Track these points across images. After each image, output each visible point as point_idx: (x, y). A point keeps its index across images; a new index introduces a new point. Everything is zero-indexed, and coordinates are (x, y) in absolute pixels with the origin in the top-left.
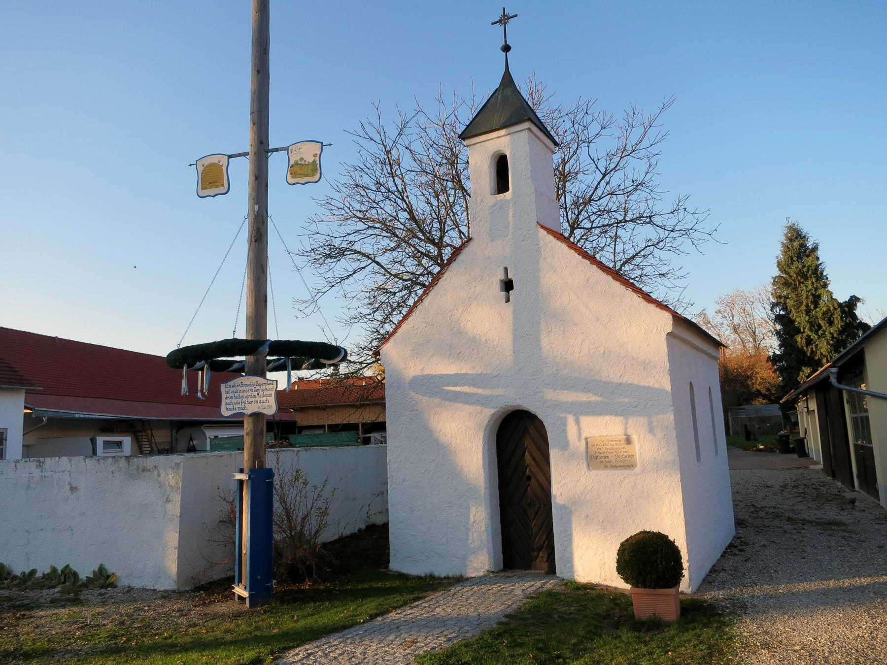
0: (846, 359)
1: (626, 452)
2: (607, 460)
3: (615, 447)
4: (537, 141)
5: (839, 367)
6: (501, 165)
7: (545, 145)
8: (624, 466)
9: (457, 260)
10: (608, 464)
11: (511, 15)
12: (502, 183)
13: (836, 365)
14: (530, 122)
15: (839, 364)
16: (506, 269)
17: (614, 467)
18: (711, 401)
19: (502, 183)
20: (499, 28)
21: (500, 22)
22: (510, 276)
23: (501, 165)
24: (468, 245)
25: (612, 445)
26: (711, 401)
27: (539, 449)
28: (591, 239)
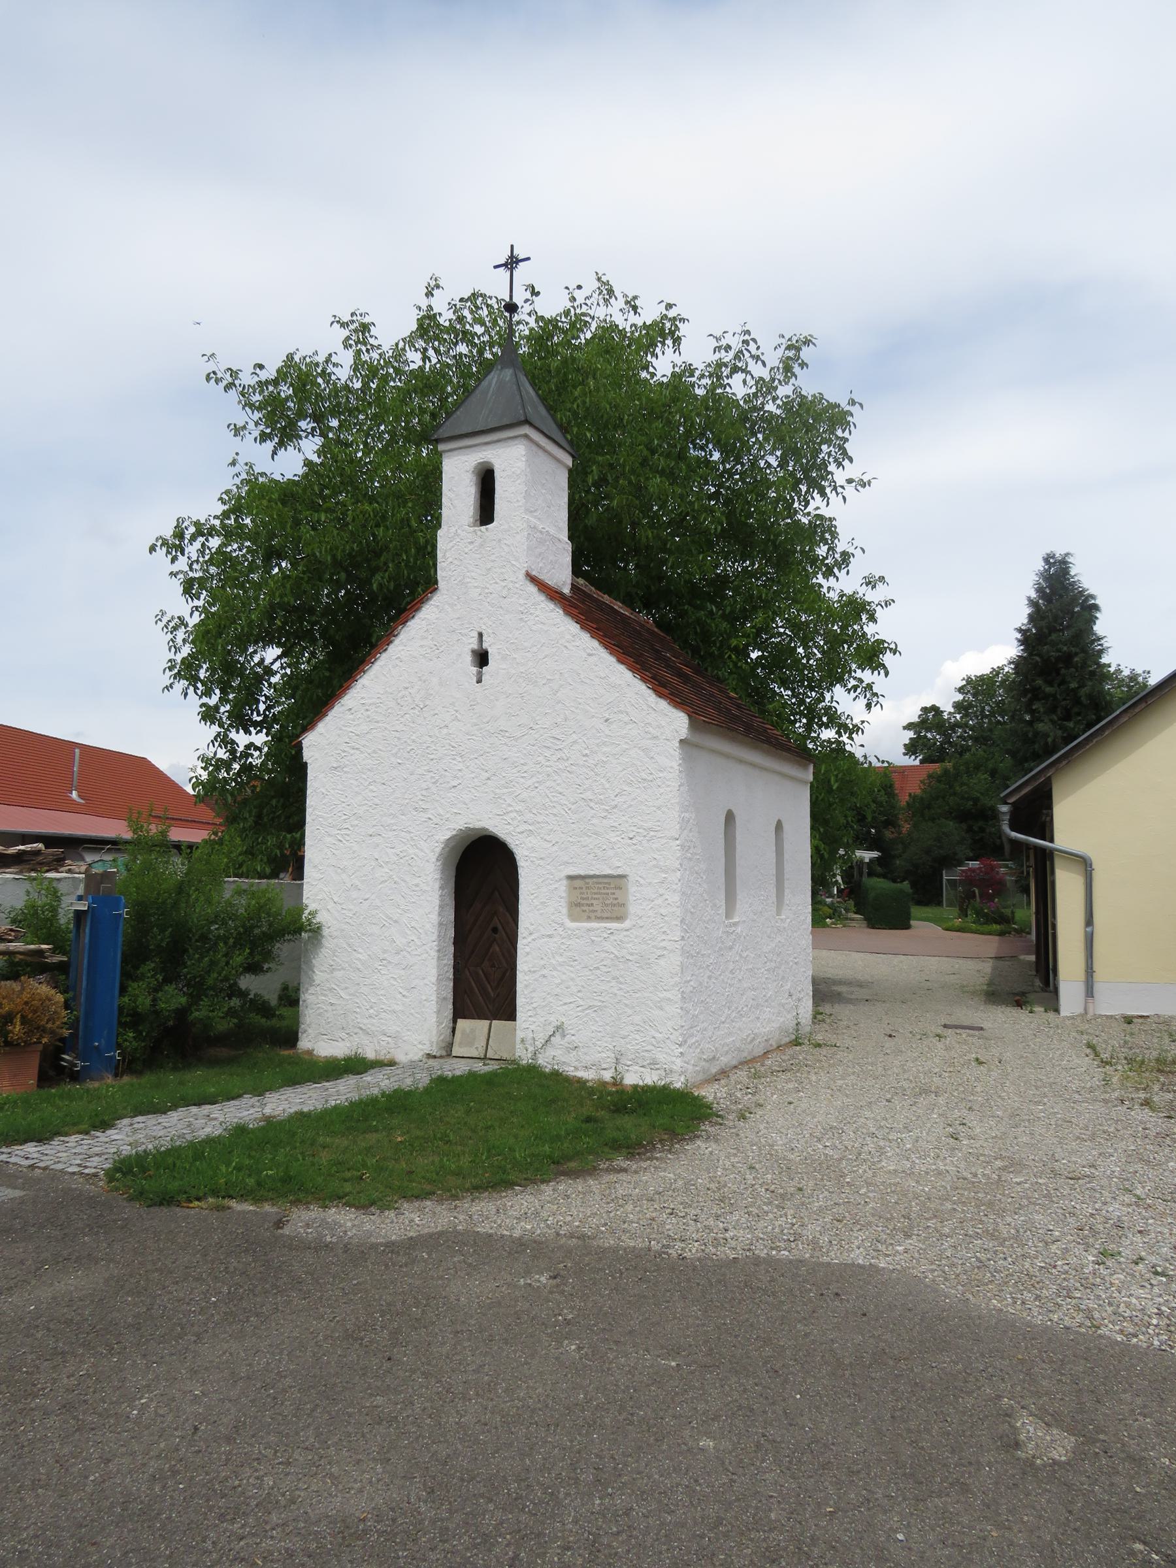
0: (1023, 792)
1: (616, 899)
2: (591, 908)
3: (603, 891)
4: (540, 453)
5: (1013, 804)
6: (486, 481)
7: (545, 451)
8: (611, 918)
9: (416, 618)
10: (592, 915)
11: (521, 257)
12: (486, 514)
13: (1009, 801)
14: (525, 442)
15: (1011, 800)
16: (481, 635)
17: (599, 918)
18: (1089, 921)
19: (486, 514)
20: (504, 274)
21: (505, 265)
22: (485, 646)
23: (486, 481)
24: (432, 597)
25: (599, 888)
26: (1089, 921)
27: (511, 943)
28: (383, 972)
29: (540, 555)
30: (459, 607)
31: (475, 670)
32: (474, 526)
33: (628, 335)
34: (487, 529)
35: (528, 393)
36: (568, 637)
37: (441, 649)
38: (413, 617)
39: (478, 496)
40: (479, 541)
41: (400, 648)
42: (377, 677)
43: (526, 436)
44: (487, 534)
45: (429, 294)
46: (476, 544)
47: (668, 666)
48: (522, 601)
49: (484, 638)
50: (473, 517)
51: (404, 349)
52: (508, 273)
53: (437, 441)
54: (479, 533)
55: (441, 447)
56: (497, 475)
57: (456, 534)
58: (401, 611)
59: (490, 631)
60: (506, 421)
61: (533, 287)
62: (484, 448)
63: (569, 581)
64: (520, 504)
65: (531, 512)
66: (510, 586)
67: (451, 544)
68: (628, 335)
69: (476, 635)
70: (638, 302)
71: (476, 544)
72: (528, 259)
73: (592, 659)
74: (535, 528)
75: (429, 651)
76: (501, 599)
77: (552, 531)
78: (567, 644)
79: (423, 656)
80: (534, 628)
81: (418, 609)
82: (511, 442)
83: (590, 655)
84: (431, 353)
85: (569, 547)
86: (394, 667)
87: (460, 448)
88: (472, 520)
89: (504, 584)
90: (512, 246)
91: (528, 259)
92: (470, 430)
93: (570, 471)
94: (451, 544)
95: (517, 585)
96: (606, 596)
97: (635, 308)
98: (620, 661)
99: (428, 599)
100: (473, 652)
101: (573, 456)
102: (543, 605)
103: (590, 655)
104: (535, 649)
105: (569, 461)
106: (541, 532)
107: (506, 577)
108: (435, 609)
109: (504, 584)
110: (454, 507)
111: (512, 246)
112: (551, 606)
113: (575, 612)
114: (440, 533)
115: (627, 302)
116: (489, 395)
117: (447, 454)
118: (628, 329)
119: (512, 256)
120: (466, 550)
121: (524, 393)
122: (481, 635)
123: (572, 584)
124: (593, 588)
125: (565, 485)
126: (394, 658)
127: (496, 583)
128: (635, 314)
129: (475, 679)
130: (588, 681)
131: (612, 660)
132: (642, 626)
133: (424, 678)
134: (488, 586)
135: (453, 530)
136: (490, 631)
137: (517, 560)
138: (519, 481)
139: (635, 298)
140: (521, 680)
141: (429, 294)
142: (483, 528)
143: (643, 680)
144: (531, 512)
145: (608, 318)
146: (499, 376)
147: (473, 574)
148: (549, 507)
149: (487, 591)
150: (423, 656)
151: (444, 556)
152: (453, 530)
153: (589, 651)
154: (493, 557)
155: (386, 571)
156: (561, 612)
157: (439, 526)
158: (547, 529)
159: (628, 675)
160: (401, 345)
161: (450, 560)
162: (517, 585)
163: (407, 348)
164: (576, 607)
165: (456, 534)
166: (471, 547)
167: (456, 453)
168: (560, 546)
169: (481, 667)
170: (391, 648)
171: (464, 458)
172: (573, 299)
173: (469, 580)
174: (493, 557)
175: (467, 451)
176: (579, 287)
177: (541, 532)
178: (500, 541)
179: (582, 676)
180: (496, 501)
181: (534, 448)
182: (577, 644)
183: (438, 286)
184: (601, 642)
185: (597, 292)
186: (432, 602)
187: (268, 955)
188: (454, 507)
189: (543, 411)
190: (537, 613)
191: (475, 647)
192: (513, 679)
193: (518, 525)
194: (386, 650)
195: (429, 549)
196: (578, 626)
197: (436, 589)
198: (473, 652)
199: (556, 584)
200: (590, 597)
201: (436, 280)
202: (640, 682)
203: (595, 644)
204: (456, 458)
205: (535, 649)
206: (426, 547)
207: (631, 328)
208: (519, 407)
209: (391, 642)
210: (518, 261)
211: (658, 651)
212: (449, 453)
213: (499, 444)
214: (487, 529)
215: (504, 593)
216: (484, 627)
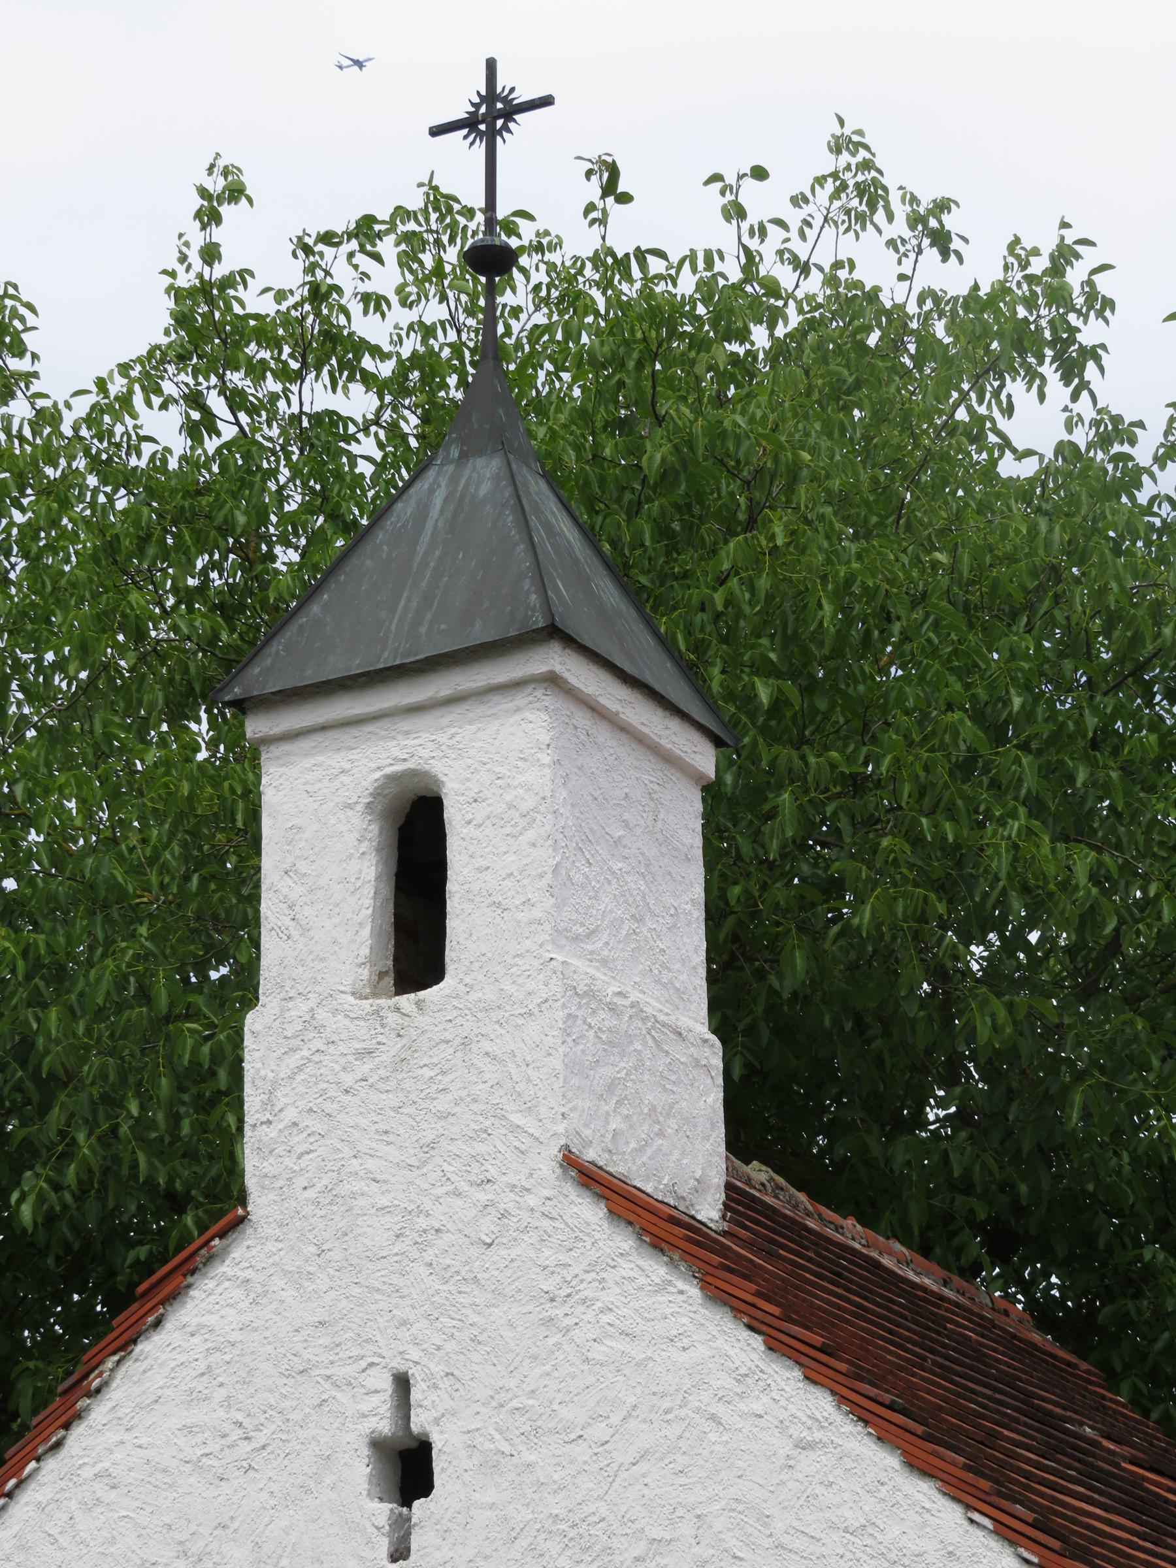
4: (603, 734)
9: (169, 1325)
11: (523, 95)
14: (549, 700)
16: (402, 1384)
21: (469, 123)
22: (419, 1421)
24: (225, 1251)
29: (610, 1088)
30: (322, 1282)
31: (383, 1511)
32: (375, 995)
33: (914, 325)
34: (419, 1004)
35: (549, 528)
36: (726, 1382)
37: (260, 1438)
38: (158, 1324)
39: (388, 891)
40: (393, 1048)
41: (112, 1437)
42: (23, 1548)
43: (553, 681)
44: (421, 1021)
45: (209, 217)
46: (386, 1056)
47: (1090, 1475)
48: (549, 1256)
49: (415, 1395)
50: (371, 961)
51: (125, 400)
52: (480, 149)
53: (242, 706)
54: (392, 1018)
55: (256, 727)
56: (451, 813)
57: (310, 1023)
58: (119, 1301)
59: (438, 1369)
60: (481, 633)
61: (614, 171)
62: (406, 724)
63: (717, 1177)
64: (537, 913)
65: (576, 938)
66: (508, 1201)
67: (293, 1061)
68: (1047, 334)
69: (384, 1383)
70: (951, 222)
71: (386, 1056)
72: (546, 101)
73: (807, 1463)
74: (590, 994)
75: (213, 1447)
76: (474, 1251)
77: (653, 1003)
78: (720, 1409)
79: (196, 1464)
80: (597, 1352)
81: (174, 1296)
82: (502, 704)
83: (809, 1446)
84: (217, 404)
85: (713, 1055)
86: (86, 1507)
87: (324, 728)
88: (365, 973)
89: (482, 1197)
90: (491, 65)
91: (546, 101)
92: (356, 666)
93: (712, 793)
94: (293, 1061)
95: (532, 1200)
96: (850, 1222)
97: (941, 241)
98: (917, 1466)
99: (210, 1259)
100: (378, 1445)
101: (718, 742)
102: (626, 1268)
103: (809, 1446)
104: (600, 1431)
105: (705, 759)
106: (612, 1008)
107: (493, 1172)
108: (238, 1294)
109: (482, 1197)
110: (305, 930)
111: (491, 65)
112: (656, 1269)
113: (746, 1290)
114: (253, 1021)
115: (915, 220)
116: (421, 548)
117: (275, 750)
118: (912, 308)
119: (491, 95)
120: (348, 1079)
121: (539, 535)
122: (402, 1384)
123: (729, 1187)
124: (802, 1197)
125: (692, 839)
126: (87, 1473)
127: (457, 1194)
128: (945, 254)
129: (383, 1546)
130: (798, 1543)
131: (885, 1462)
132: (985, 1326)
133: (195, 1548)
134: (428, 1205)
135: (300, 1008)
136: (438, 1369)
137: (530, 1110)
138: (530, 835)
139: (942, 206)
140: (554, 1546)
141: (209, 217)
142: (406, 1001)
143: (1006, 1532)
144: (576, 938)
145: (843, 274)
146: (454, 480)
147: (371, 1164)
148: (639, 920)
149: (422, 1222)
150: (196, 1464)
151: (268, 1104)
152: (300, 1008)
153: (796, 1431)
154: (443, 1104)
155: (65, 1157)
156: (694, 1291)
157: (250, 999)
158: (635, 996)
159: (950, 1514)
160: (117, 386)
161: (291, 1114)
162: (532, 1200)
163: (138, 399)
164: (748, 1273)
165: (310, 1023)
166: (365, 1068)
167: (306, 744)
168: (680, 1053)
169: (407, 1502)
170: (79, 1438)
171: (337, 761)
172: (736, 212)
173: (357, 1186)
174: (443, 1104)
175: (346, 736)
176: (759, 173)
177: (612, 1008)
178: (466, 1043)
179: (778, 1526)
180: (453, 905)
181: (582, 719)
182: (757, 1408)
183: (236, 192)
184: (842, 1399)
185: (830, 186)
186: (224, 1268)
187: (358, 224)
188: (305, 930)
189: (609, 592)
190: (610, 1296)
191: (384, 1426)
192: (523, 1543)
193: (531, 985)
194: (59, 1445)
195: (223, 1075)
196: (757, 1341)
197: (242, 1220)
198: (378, 1445)
199: (672, 1189)
200: (795, 1229)
201: (226, 173)
202: (994, 1544)
203: (822, 1403)
204: (308, 763)
205: (600, 1431)
206: (213, 1074)
207: (921, 301)
208: (527, 584)
209: (78, 1416)
210: (512, 110)
211: (1046, 1419)
212: (286, 747)
213: (459, 710)
214: (419, 1004)
215: (487, 1226)
216: (414, 1354)
